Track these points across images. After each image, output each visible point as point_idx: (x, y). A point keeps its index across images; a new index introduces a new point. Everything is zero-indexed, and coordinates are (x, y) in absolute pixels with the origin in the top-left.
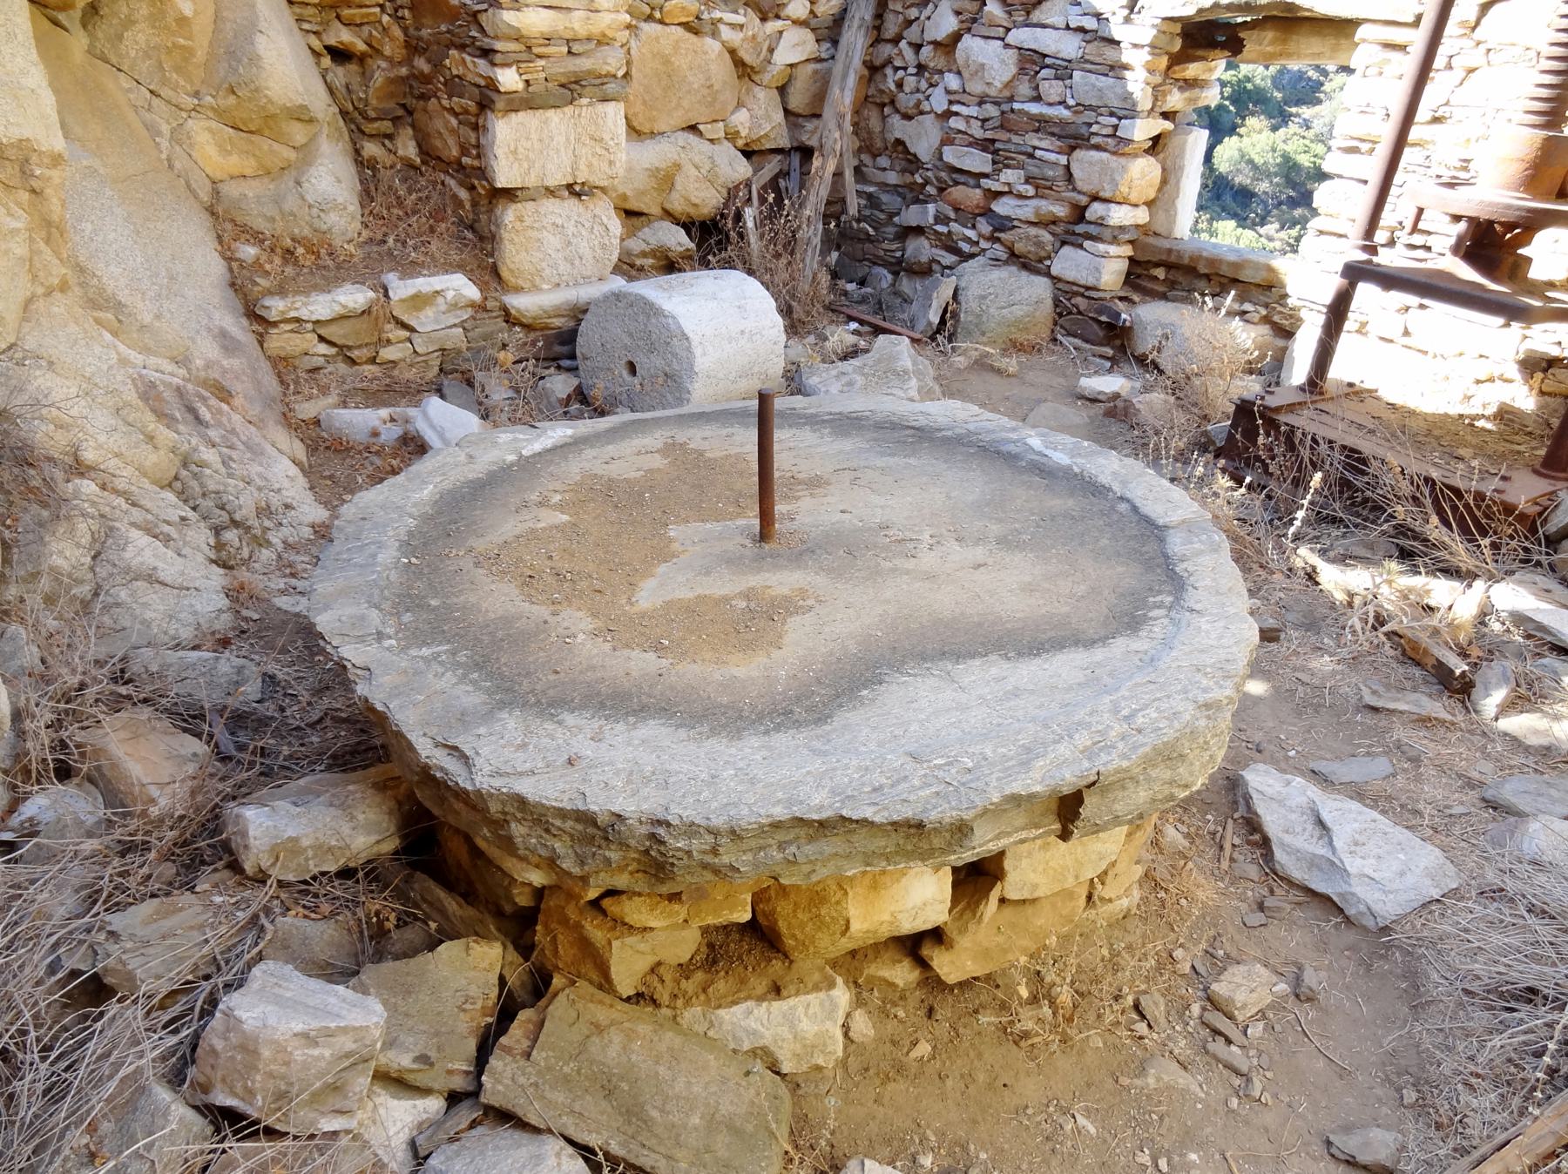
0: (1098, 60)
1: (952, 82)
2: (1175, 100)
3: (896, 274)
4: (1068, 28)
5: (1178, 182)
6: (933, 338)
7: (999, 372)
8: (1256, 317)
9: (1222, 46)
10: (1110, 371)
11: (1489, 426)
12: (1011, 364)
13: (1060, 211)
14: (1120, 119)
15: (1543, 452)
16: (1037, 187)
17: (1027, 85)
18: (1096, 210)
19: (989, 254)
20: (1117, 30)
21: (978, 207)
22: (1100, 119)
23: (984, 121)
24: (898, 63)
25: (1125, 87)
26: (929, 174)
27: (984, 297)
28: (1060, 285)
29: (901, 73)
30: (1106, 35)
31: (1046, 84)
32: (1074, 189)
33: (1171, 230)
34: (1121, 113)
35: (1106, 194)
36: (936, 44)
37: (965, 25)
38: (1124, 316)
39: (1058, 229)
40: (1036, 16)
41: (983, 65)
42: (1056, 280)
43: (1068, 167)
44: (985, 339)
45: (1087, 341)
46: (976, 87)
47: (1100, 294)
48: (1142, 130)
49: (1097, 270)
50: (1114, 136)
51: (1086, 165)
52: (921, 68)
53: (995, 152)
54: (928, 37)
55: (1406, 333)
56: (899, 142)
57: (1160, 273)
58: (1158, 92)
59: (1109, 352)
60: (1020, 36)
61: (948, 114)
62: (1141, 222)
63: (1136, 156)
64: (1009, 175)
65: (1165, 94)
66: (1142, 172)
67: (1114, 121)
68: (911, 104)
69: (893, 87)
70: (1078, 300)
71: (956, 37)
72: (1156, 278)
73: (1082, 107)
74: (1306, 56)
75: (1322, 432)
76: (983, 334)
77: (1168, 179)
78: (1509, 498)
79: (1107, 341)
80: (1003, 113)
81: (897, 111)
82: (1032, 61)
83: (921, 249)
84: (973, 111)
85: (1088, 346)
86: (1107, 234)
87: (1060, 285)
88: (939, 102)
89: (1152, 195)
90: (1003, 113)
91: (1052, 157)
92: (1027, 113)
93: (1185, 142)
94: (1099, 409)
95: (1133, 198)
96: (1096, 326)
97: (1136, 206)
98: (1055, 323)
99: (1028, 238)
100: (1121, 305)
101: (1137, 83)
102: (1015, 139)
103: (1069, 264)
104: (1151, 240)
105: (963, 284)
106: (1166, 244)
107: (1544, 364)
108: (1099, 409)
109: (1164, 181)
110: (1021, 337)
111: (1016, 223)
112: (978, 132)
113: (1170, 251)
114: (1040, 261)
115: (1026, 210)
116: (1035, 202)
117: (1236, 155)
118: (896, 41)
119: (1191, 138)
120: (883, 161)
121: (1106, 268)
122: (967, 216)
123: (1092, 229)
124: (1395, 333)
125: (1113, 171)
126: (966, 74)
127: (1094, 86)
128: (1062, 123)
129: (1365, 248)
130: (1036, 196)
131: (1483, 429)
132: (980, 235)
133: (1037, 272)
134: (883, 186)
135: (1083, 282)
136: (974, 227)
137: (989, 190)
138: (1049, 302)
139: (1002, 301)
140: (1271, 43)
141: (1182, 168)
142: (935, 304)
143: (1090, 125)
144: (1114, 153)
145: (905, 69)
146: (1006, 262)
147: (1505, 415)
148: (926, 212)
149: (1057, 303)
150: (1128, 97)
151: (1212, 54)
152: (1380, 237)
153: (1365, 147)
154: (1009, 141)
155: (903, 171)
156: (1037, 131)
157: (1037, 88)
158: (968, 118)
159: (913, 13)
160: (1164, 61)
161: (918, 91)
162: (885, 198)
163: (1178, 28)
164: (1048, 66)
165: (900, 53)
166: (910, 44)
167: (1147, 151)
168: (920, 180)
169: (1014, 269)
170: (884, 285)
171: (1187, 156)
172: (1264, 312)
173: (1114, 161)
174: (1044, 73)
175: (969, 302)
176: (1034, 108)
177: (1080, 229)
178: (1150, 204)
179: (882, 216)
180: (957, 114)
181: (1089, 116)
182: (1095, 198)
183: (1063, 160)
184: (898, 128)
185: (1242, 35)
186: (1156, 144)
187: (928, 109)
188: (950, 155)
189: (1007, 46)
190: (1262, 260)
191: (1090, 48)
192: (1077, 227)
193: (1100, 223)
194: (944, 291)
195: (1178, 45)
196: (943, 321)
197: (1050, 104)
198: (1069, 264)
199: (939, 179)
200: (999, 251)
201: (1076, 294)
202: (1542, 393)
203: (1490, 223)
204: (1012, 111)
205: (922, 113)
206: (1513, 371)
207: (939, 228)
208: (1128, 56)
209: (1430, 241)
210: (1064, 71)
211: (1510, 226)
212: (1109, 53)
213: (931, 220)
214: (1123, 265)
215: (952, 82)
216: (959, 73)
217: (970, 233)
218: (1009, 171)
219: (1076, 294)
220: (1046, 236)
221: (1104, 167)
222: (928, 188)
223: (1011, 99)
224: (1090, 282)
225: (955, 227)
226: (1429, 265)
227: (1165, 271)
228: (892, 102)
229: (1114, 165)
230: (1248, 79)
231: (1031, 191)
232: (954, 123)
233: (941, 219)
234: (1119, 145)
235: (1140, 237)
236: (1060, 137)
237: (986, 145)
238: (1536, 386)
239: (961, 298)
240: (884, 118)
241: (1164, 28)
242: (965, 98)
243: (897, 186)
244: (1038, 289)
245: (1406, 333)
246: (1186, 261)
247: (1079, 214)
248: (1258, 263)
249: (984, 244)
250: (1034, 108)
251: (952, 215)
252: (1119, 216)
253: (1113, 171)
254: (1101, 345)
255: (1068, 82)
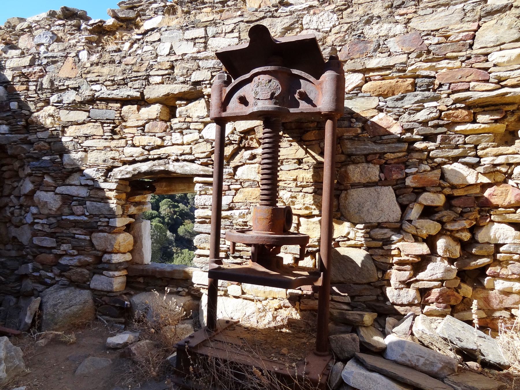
0: (96, 196)
1: (34, 210)
2: (133, 210)
3: (18, 298)
4: (81, 185)
5: (141, 241)
6: (29, 331)
7: (65, 343)
8: (184, 293)
9: (148, 189)
10: (125, 329)
11: (178, 102)
12: (72, 337)
13: (89, 259)
14: (109, 219)
15: (314, 341)
16: (78, 250)
17: (67, 208)
18: (107, 257)
19: (60, 283)
20: (103, 185)
21: (52, 262)
22: (101, 219)
23: (50, 225)
24: (10, 205)
25: (109, 206)
26: (28, 250)
27: (55, 305)
28: (96, 293)
29: (12, 209)
30: (97, 186)
31: (75, 207)
32: (95, 249)
33: (143, 261)
34: (109, 216)
35: (110, 250)
36: (26, 195)
37: (36, 187)
38: (126, 302)
39: (91, 268)
40: (67, 181)
41: (46, 202)
42: (93, 290)
43: (91, 240)
44: (57, 327)
45: (112, 317)
46: (46, 212)
47: (114, 294)
48: (120, 223)
49: (111, 283)
50: (108, 226)
51: (99, 239)
52: (21, 206)
53: (57, 238)
54: (22, 193)
55: (243, 293)
56: (15, 238)
57: (141, 280)
58: (124, 207)
59: (123, 320)
60: (59, 190)
61: (33, 224)
62: (128, 260)
63: (119, 233)
64: (64, 247)
65: (128, 208)
66: (124, 240)
67: (107, 220)
68: (18, 221)
69: (9, 214)
70: (105, 298)
71: (33, 192)
72: (140, 282)
73: (91, 216)
74: (179, 190)
75: (220, 355)
76: (56, 324)
77: (137, 241)
78: (313, 376)
79: (121, 315)
80: (58, 221)
81: (13, 225)
82: (67, 199)
83: (29, 285)
84: (45, 221)
85: (112, 319)
86: (113, 267)
87: (96, 293)
88: (29, 219)
89: (131, 248)
90: (58, 221)
91: (83, 237)
92: (69, 220)
93: (141, 225)
94: (117, 354)
95: (122, 250)
96: (115, 309)
97: (124, 253)
98: (96, 311)
99: (77, 273)
100: (125, 297)
101: (113, 204)
102: (65, 231)
103: (98, 282)
104: (135, 266)
105: (45, 300)
106: (141, 267)
107: (298, 298)
108: (117, 354)
109: (135, 242)
110: (77, 321)
111: (70, 267)
112: (47, 229)
113: (143, 270)
114: (85, 283)
115: (75, 261)
116: (78, 257)
117: (184, 231)
118: (9, 196)
119: (143, 224)
120: (9, 247)
121: (117, 281)
122: (48, 267)
123: (106, 266)
124: (239, 293)
125: (110, 240)
126: (40, 207)
127: (96, 207)
128: (85, 222)
129: (216, 262)
130: (78, 254)
131: (286, 333)
132: (55, 275)
133: (84, 288)
134: (10, 258)
135: (105, 290)
136: (52, 272)
137: (56, 254)
138: (91, 301)
139: (66, 305)
140: (165, 187)
141: (141, 236)
142: (28, 313)
143: (97, 222)
144: (109, 233)
145: (14, 207)
146: (69, 286)
147: (291, 323)
148: (28, 267)
149: (95, 301)
150: (111, 209)
151: (144, 193)
152: (222, 255)
153: (208, 220)
154: (62, 232)
155: (18, 250)
156: (74, 227)
157: (72, 210)
158: (43, 224)
159: (15, 184)
160: (124, 196)
161: (21, 215)
162: (9, 263)
163: (127, 183)
164: (75, 200)
165: (11, 201)
166: (16, 197)
167: (125, 231)
168: (25, 253)
169: (73, 288)
170: (12, 304)
171: (143, 231)
172: (187, 290)
173: (110, 236)
174: (74, 203)
175: (48, 309)
176: (72, 218)
177: (100, 266)
178: (131, 252)
179: (8, 271)
180: (38, 223)
181: (96, 219)
182: (105, 252)
183: (88, 238)
184: (14, 231)
185: (154, 184)
186: (128, 228)
187: (25, 222)
188: (36, 241)
189: (56, 194)
190: (181, 269)
191: (91, 192)
192: (100, 265)
193: (109, 262)
194: (35, 303)
195: (129, 190)
196: (34, 321)
197: (79, 216)
198: (98, 282)
199: (33, 252)
200: (64, 281)
201: (104, 295)
202: (301, 310)
203: (263, 245)
204: (62, 219)
205: (24, 224)
206: (287, 303)
207: (35, 274)
208: (108, 194)
209: (242, 254)
210: (82, 201)
211: (271, 246)
212: (100, 193)
213: (31, 271)
214: (124, 279)
215: (34, 210)
216: (37, 206)
217: (50, 274)
218: (64, 245)
219: (104, 295)
220: (86, 271)
221: (106, 239)
222: (28, 256)
223: (62, 215)
224: (109, 289)
225: (43, 272)
226: (244, 266)
227: (141, 279)
228: (10, 221)
229: (110, 237)
230: (183, 210)
231: (76, 252)
232: (36, 227)
233: (35, 270)
234: (112, 230)
235: (128, 266)
236: (85, 229)
237: (51, 235)
238: (298, 308)
239: (44, 308)
240: (7, 228)
241: (121, 183)
242: (40, 216)
243: (16, 257)
244: (85, 295)
245: (243, 293)
246: (150, 274)
247: (99, 259)
248: (179, 271)
249: (57, 279)
250: (72, 218)
251: (41, 267)
252: (117, 258)
253: (110, 240)
254: (119, 317)
255: (84, 206)
